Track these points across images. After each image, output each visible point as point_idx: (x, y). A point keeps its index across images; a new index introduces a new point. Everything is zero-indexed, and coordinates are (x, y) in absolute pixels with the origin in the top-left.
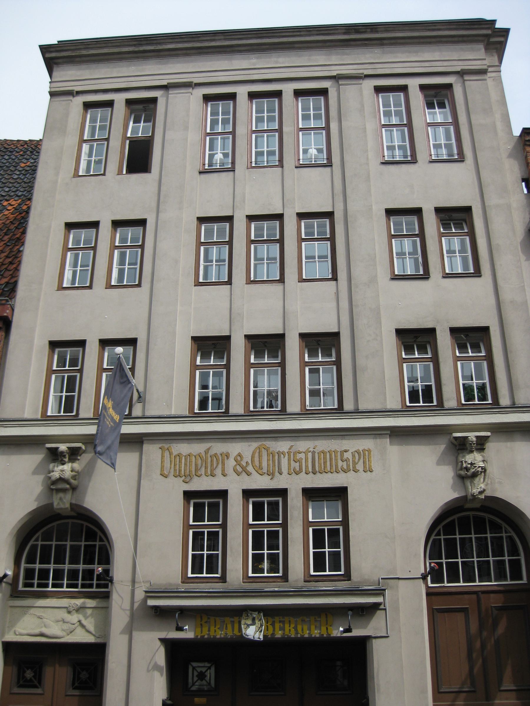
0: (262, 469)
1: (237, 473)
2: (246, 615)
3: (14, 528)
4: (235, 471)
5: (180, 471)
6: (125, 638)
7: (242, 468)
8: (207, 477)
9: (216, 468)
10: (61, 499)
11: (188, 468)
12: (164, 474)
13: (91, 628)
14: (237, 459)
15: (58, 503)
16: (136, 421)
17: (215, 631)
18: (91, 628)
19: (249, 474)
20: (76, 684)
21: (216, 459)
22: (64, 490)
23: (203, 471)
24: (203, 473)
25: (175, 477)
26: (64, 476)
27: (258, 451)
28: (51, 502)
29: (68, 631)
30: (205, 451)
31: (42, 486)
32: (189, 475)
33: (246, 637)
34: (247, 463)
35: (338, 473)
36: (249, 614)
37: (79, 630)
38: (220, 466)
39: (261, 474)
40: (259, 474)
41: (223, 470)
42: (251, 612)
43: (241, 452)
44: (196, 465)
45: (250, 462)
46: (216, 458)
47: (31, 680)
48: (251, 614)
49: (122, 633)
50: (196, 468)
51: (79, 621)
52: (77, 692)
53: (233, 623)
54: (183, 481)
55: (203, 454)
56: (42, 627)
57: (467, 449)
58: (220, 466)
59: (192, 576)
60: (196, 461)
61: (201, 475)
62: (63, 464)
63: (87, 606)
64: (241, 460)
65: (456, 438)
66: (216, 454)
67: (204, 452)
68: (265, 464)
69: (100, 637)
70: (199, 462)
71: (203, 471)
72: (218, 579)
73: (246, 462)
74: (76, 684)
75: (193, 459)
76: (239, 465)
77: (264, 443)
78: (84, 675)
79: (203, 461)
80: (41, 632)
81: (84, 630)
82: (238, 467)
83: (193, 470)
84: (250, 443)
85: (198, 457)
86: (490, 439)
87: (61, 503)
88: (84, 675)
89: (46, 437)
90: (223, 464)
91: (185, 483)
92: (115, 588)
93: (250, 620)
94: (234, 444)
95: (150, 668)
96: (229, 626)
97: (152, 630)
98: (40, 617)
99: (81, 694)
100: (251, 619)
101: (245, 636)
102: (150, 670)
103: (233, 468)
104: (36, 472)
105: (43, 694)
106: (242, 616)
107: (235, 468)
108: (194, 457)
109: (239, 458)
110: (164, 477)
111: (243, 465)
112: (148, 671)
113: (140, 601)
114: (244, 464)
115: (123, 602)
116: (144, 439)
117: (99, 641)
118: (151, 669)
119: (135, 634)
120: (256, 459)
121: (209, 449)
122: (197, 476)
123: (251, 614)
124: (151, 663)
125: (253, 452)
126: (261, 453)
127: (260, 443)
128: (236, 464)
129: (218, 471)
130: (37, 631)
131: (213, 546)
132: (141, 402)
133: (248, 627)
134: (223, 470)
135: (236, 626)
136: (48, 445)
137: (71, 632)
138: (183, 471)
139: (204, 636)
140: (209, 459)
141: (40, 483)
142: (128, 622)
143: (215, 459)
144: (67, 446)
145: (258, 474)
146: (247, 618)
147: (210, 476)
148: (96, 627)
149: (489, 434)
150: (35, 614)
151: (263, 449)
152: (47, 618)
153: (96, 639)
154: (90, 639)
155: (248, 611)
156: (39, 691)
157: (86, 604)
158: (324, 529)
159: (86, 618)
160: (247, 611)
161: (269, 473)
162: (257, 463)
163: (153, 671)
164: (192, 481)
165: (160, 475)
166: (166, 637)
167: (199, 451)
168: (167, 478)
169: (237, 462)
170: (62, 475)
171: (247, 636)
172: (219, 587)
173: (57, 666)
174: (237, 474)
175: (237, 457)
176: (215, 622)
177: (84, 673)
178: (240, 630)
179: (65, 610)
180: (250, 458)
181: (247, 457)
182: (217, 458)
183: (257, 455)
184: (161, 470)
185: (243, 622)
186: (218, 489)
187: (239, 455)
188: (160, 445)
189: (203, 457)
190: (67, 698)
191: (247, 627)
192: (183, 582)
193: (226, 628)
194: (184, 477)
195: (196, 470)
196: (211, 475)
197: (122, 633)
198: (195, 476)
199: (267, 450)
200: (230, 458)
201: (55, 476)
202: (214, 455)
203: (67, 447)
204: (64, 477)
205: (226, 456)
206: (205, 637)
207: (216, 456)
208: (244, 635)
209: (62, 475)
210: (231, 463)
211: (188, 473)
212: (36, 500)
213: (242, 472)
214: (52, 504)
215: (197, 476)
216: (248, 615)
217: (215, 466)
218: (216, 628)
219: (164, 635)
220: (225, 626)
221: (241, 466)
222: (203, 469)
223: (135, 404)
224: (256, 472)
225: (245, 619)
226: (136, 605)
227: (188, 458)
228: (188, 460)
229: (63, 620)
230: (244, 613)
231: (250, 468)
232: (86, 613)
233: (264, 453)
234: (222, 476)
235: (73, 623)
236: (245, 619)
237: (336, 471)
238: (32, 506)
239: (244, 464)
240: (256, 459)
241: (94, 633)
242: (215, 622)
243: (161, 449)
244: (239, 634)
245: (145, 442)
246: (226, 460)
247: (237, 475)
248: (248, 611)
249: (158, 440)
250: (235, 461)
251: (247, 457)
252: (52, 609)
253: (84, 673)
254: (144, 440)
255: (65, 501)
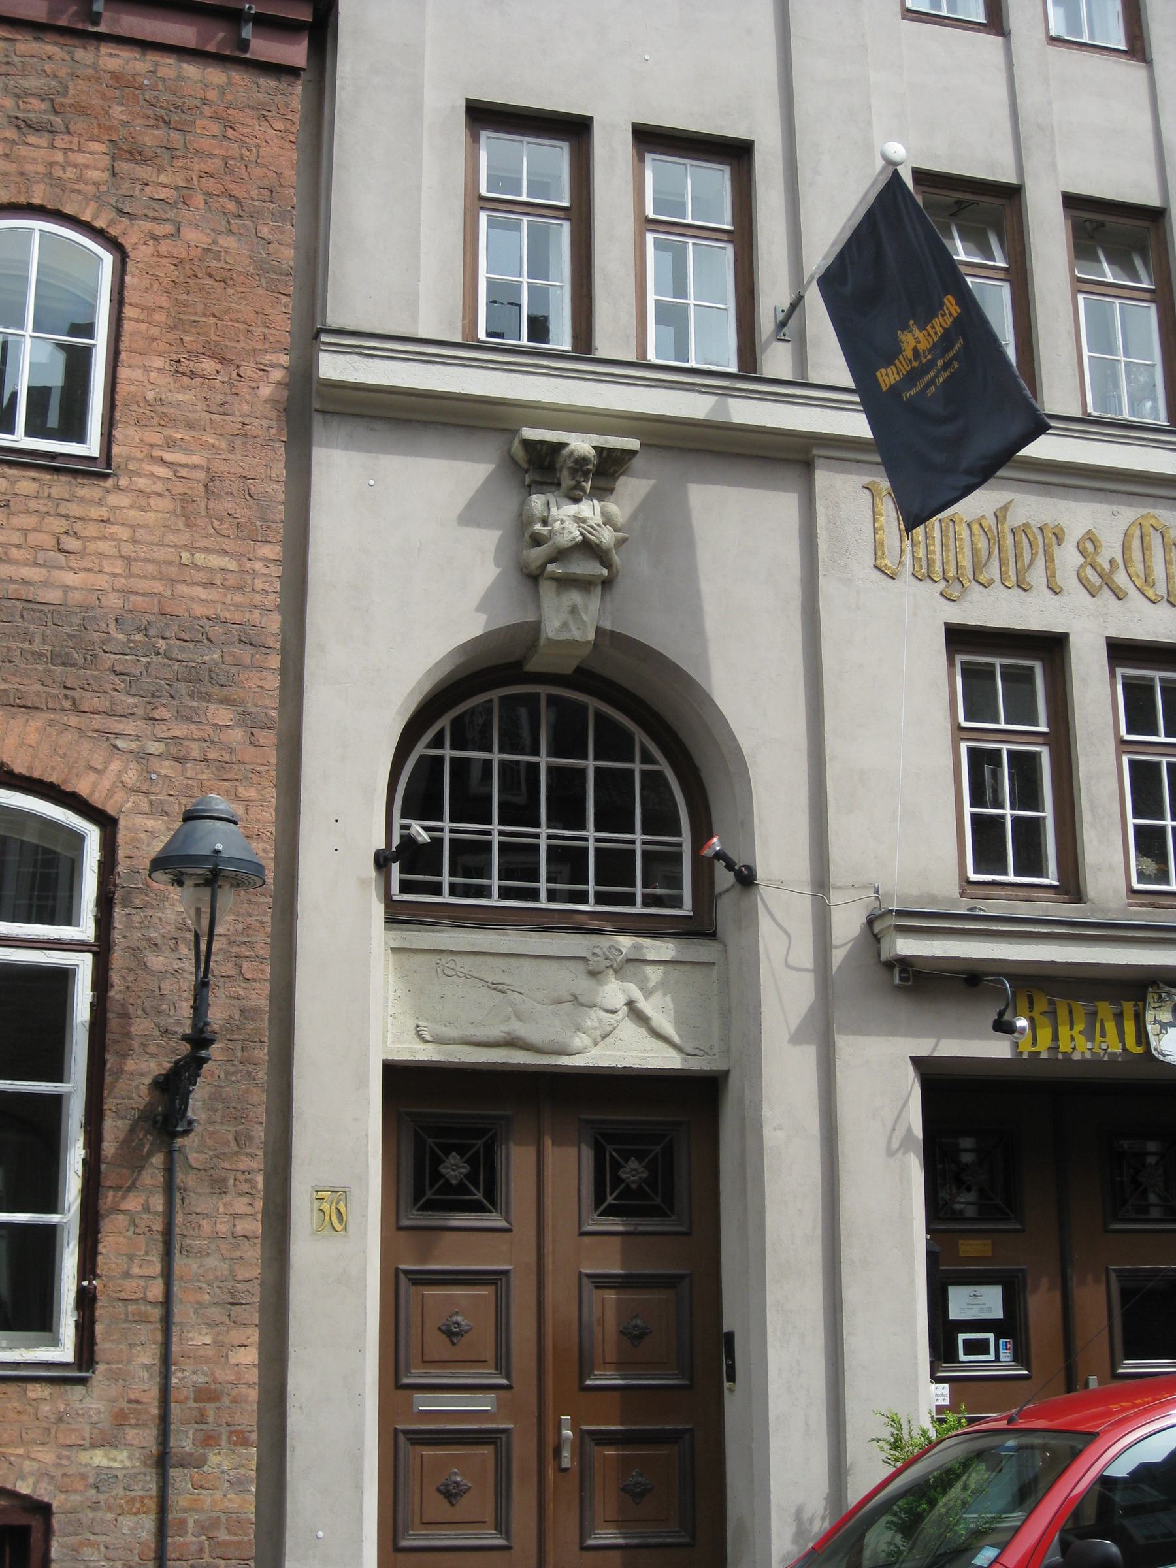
0: (1154, 585)
1: (1091, 590)
2: (1156, 997)
3: (412, 693)
4: (1083, 581)
5: (930, 563)
6: (807, 1056)
7: (1101, 578)
8: (1007, 590)
9: (1029, 567)
10: (574, 610)
11: (952, 555)
12: (886, 565)
13: (664, 1023)
14: (1085, 549)
15: (565, 625)
16: (799, 394)
17: (1072, 1038)
18: (664, 1023)
19: (1119, 595)
20: (610, 1200)
21: (1027, 541)
22: (583, 584)
23: (994, 570)
24: (997, 578)
25: (916, 581)
26: (598, 538)
27: (1138, 533)
28: (531, 617)
29: (597, 1034)
30: (995, 513)
31: (497, 565)
32: (958, 578)
33: (1161, 1058)
34: (1112, 562)
35: (936, 582)
36: (1163, 995)
37: (629, 1031)
38: (1040, 562)
39: (1153, 598)
40: (1147, 598)
41: (1050, 576)
42: (1167, 989)
43: (1094, 530)
44: (974, 551)
45: (1119, 560)
46: (1028, 538)
47: (461, 1189)
48: (1169, 994)
49: (797, 1038)
50: (976, 559)
51: (630, 1004)
52: (615, 1224)
53: (1119, 1017)
54: (942, 594)
55: (990, 522)
56: (508, 1019)
57: (559, 485)
58: (1040, 562)
59: (981, 880)
60: (973, 539)
61: (992, 582)
62: (576, 500)
63: (648, 958)
64: (1096, 552)
65: (528, 444)
66: (1027, 525)
67: (994, 516)
68: (1159, 572)
69: (697, 1052)
70: (982, 544)
71: (994, 570)
72: (1053, 891)
73: (1110, 561)
74: (610, 1200)
75: (965, 534)
76: (1092, 566)
77: (1152, 511)
78: (633, 1171)
79: (992, 541)
80: (508, 1033)
81: (643, 1032)
82: (1090, 572)
83: (967, 562)
84: (1115, 508)
85: (976, 527)
86: (637, 463)
87: (573, 627)
88: (633, 1171)
89: (503, 408)
90: (1049, 558)
91: (947, 602)
92: (762, 899)
93: (1168, 1011)
94: (1072, 505)
95: (895, 1144)
96: (1111, 1027)
97: (893, 1032)
98: (494, 987)
99: (631, 1228)
100: (1171, 1009)
101: (1157, 1056)
102: (898, 1150)
103: (1075, 572)
104: (470, 516)
105: (508, 1230)
106: (1144, 999)
107: (1082, 575)
108: (964, 525)
109: (1089, 545)
110: (884, 577)
111: (1104, 569)
112: (891, 1153)
113: (851, 944)
114: (1107, 566)
115: (790, 943)
116: (815, 452)
117: (696, 1064)
118: (900, 1146)
119: (845, 1044)
120: (1136, 554)
121: (1005, 509)
122: (981, 584)
123: (1169, 994)
124: (897, 1128)
125: (1125, 534)
126: (1146, 539)
127: (1142, 511)
128: (1085, 562)
129: (1037, 576)
130: (496, 1031)
131: (1027, 794)
132: (789, 341)
133: (1163, 1031)
134: (1050, 576)
135: (1130, 1026)
136: (530, 433)
137: (604, 1037)
138: (938, 564)
139: (1039, 1053)
140: (1009, 541)
141: (490, 556)
142: (811, 1009)
143: (1025, 541)
144: (594, 444)
145: (1145, 600)
146: (1159, 1004)
147: (1164, 603)
148: (680, 1021)
149: (633, 444)
150: (482, 976)
151: (1151, 529)
152: (522, 991)
153: (685, 1060)
154: (665, 1059)
155: (1161, 985)
156: (494, 1220)
157: (645, 950)
158: (1158, 764)
159: (648, 994)
160: (1158, 985)
161: (1172, 599)
162: (1138, 567)
163: (904, 1154)
164: (969, 599)
165: (875, 570)
166: (933, 1051)
167: (979, 512)
168: (894, 579)
169: (1085, 558)
170: (590, 533)
171: (1164, 1055)
172: (1066, 910)
173: (548, 1142)
174: (1088, 590)
175: (1084, 543)
176: (1071, 1012)
177: (633, 1164)
178: (1142, 1036)
179: (581, 967)
180: (1120, 550)
181: (1111, 549)
182: (1032, 540)
183: (1136, 543)
184: (876, 554)
185: (1150, 1015)
186: (1040, 630)
187: (1090, 537)
188: (867, 480)
189: (991, 529)
190: (586, 1239)
191: (1160, 1031)
192: (962, 895)
193: (1103, 1034)
194: (943, 584)
195: (977, 567)
196: (1019, 586)
197: (797, 1038)
198: (973, 581)
199: (1161, 532)
200: (1065, 543)
201: (571, 533)
202: (1022, 528)
203: (594, 447)
204: (598, 542)
205: (1054, 538)
206: (1041, 1057)
207: (1028, 531)
208: (1154, 1052)
209: (590, 533)
210: (1069, 558)
211: (952, 573)
212: (479, 609)
213: (1101, 587)
214: (535, 628)
215: (981, 584)
216: (1160, 997)
217: (1027, 557)
218: (1075, 1032)
219: (924, 1047)
220: (1098, 1026)
221: (1098, 569)
222: (995, 564)
223: (768, 343)
224: (1138, 592)
225: (1155, 1008)
226: (838, 956)
227: (951, 529)
228: (951, 534)
229: (575, 997)
230: (1150, 990)
231: (1121, 578)
232: (646, 979)
233: (1156, 541)
234: (1049, 592)
235: (611, 1008)
236: (1155, 1008)
237: (1018, 586)
238: (472, 627)
239: (1107, 566)
240: (1136, 554)
241: (676, 1039)
242: (1071, 1012)
243: (867, 492)
244: (1140, 1050)
245: (818, 462)
246: (1055, 547)
247: (1089, 596)
248: (1161, 985)
249: (858, 461)
250: (1079, 555)
251: (1111, 549)
252: (534, 962)
253: (633, 1164)
254: (815, 456)
255: (585, 618)
